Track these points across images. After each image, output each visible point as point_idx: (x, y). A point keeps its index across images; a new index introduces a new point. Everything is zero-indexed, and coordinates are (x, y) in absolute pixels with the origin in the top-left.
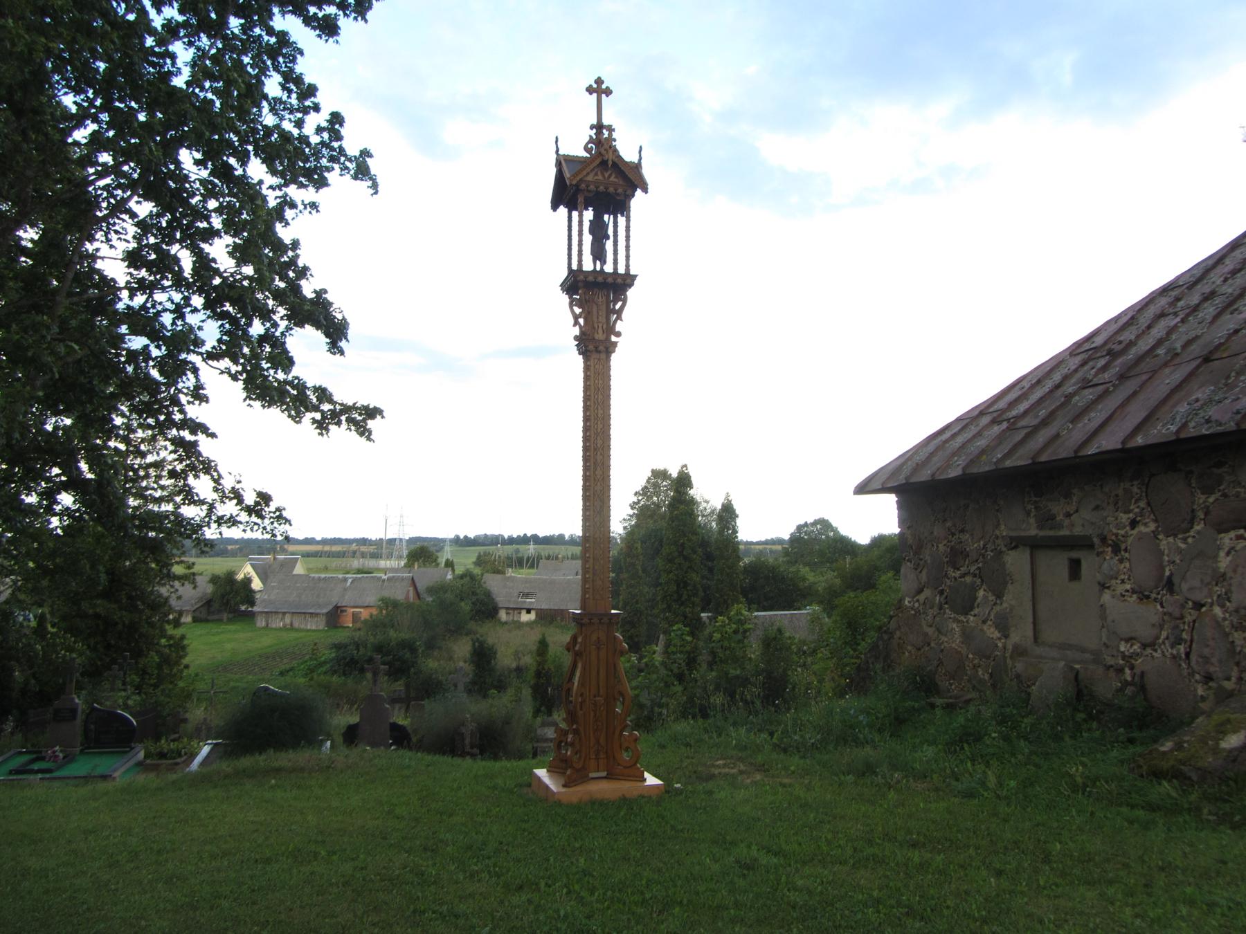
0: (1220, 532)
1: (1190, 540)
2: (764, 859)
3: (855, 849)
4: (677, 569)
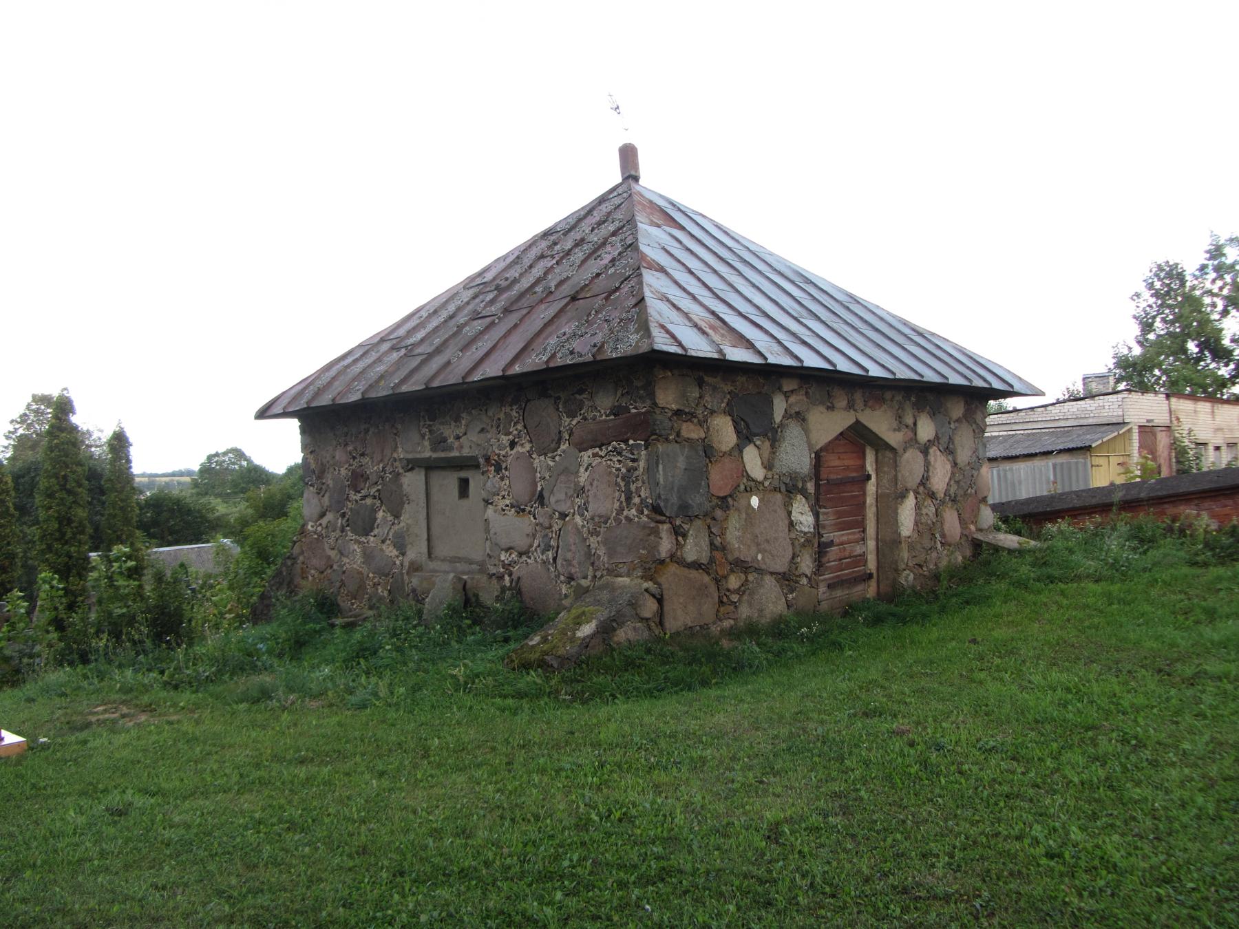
0: (580, 451)
1: (557, 458)
2: (140, 801)
3: (241, 776)
4: (58, 505)
